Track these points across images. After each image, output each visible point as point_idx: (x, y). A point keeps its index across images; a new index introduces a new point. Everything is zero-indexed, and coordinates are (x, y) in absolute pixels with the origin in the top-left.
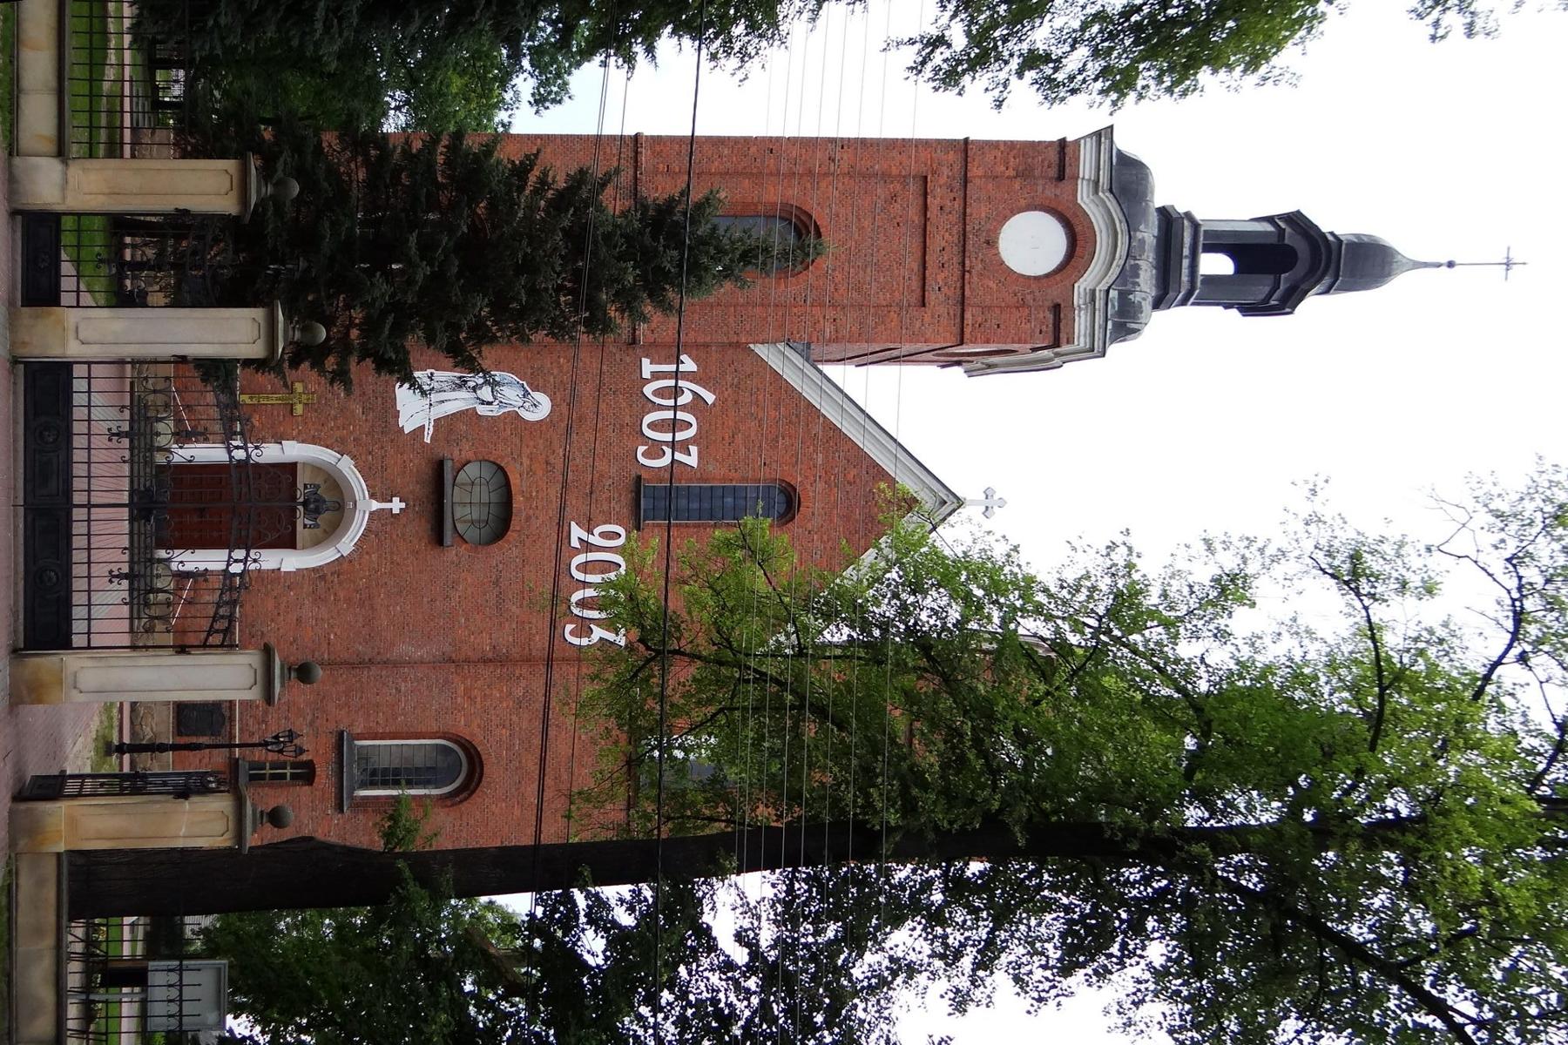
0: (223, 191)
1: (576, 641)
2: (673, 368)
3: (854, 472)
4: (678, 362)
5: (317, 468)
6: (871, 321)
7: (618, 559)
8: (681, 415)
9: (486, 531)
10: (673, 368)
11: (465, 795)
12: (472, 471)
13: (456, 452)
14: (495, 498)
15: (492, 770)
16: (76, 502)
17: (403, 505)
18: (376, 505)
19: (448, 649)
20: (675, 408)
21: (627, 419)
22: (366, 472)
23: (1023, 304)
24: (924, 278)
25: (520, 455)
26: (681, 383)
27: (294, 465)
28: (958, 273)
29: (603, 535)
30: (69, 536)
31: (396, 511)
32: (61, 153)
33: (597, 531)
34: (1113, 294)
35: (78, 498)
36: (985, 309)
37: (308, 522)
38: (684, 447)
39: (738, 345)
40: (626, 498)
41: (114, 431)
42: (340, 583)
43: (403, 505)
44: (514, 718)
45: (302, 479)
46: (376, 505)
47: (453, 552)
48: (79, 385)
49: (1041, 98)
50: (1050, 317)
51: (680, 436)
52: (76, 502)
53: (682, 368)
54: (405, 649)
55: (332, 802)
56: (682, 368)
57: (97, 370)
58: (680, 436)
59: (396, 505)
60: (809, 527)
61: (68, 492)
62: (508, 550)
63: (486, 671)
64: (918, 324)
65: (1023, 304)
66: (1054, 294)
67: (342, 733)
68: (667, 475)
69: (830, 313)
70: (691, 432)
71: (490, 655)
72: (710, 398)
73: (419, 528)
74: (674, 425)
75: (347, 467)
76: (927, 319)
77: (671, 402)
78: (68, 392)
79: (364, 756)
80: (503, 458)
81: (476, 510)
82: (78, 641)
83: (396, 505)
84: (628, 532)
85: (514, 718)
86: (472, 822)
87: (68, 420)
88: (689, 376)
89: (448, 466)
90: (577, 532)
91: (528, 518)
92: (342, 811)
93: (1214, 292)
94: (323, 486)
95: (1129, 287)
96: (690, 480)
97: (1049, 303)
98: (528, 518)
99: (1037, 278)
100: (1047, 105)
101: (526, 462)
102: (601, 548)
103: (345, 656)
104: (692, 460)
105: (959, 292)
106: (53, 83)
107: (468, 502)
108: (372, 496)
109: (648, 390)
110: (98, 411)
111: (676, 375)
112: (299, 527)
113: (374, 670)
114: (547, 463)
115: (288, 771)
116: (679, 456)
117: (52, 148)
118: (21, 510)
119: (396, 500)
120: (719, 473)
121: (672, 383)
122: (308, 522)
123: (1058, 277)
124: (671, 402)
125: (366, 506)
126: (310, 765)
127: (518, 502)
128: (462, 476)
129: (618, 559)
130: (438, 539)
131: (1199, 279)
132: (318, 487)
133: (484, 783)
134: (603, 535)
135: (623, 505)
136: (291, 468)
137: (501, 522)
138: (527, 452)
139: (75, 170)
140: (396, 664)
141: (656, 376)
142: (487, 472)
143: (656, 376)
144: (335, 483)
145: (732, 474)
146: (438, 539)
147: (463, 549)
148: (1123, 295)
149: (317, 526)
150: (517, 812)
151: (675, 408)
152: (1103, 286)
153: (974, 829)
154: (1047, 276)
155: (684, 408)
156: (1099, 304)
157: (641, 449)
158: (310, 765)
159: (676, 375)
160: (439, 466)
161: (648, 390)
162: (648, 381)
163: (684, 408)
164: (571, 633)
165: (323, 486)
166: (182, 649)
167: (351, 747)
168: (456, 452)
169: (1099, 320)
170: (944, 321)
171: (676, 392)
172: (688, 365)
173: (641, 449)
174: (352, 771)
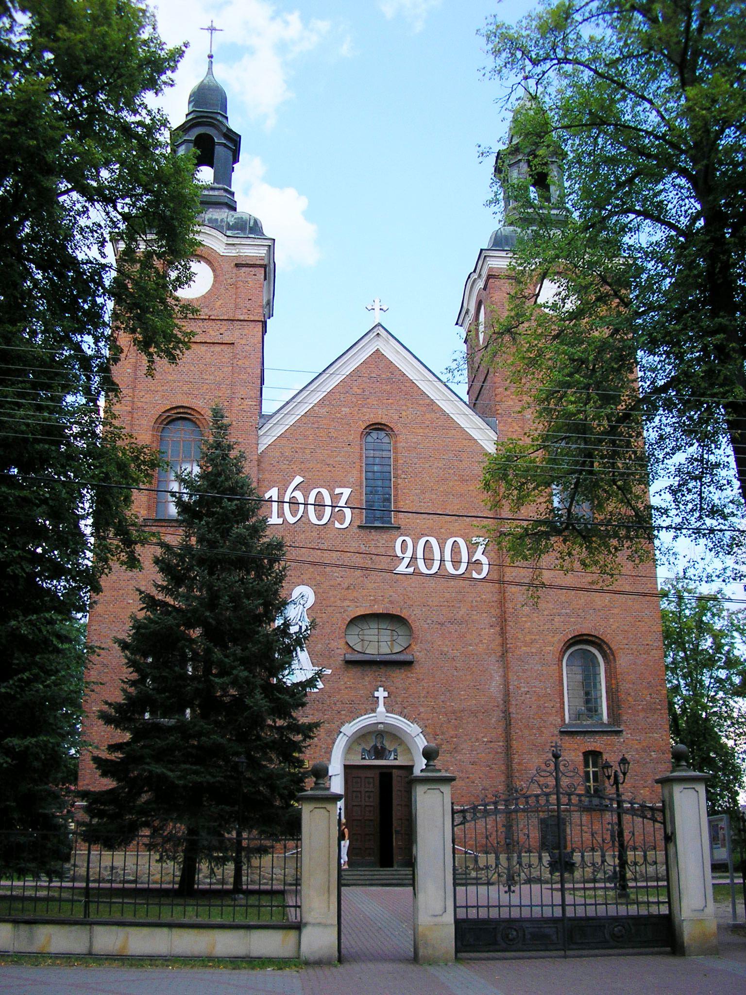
0: (327, 814)
1: (486, 568)
2: (275, 505)
3: (355, 389)
4: (270, 500)
5: (349, 749)
6: (244, 377)
7: (450, 542)
8: (311, 500)
9: (401, 630)
10: (275, 505)
11: (605, 646)
12: (353, 640)
13: (339, 651)
14: (374, 625)
15: (586, 627)
16: (560, 915)
17: (381, 689)
18: (381, 708)
19: (493, 659)
20: (306, 504)
21: (315, 534)
22: (354, 715)
23: (234, 285)
24: (214, 343)
25: (342, 607)
26: (287, 499)
27: (346, 767)
28: (210, 323)
29: (404, 551)
30: (587, 919)
31: (386, 694)
32: (298, 927)
33: (399, 554)
34: (229, 233)
35: (558, 912)
36: (236, 306)
37: (392, 757)
38: (335, 497)
39: (259, 462)
40: (374, 534)
41: (507, 889)
42: (443, 734)
43: (381, 689)
44: (546, 613)
45: (356, 760)
46: (381, 708)
47: (418, 653)
48: (472, 914)
49: (186, 286)
50: (244, 269)
51: (328, 501)
52: (560, 915)
53: (275, 498)
54: (495, 686)
55: (614, 738)
56: (275, 498)
57: (461, 902)
58: (328, 501)
59: (381, 694)
60: (397, 417)
61: (553, 920)
62: (411, 614)
63: (511, 631)
64: (248, 347)
65: (234, 285)
66: (228, 267)
67: (562, 732)
68: (356, 511)
69: (237, 401)
70: (325, 493)
71: (498, 629)
72: (298, 479)
73: (398, 677)
74: (319, 505)
75: (350, 729)
76: (243, 342)
77: (302, 507)
78: (478, 921)
79: (578, 716)
80: (344, 619)
81: (382, 638)
82: (664, 910)
83: (381, 694)
84: (402, 535)
85: (546, 613)
86: (625, 642)
87: (499, 922)
88: (282, 493)
89: (349, 657)
90: (402, 568)
91: (391, 602)
92: (621, 731)
93: (224, 177)
94: (364, 746)
95: (224, 224)
96: (361, 493)
97: (235, 270)
98: (391, 602)
99: (215, 276)
100: (191, 283)
101: (347, 603)
102: (413, 552)
103: (500, 731)
104: (347, 492)
105: (224, 323)
106: (242, 932)
107: (379, 643)
108: (374, 710)
109: (292, 520)
110: (491, 899)
111: (281, 502)
112: (396, 763)
113: (512, 710)
114: (348, 588)
115: (591, 769)
116: (342, 503)
117: (292, 934)
118: (569, 953)
119: (376, 694)
120: (354, 476)
121: (286, 506)
122: (392, 757)
123: (216, 264)
124: (302, 507)
125: (381, 715)
126: (586, 754)
127: (378, 609)
128: (358, 648)
129: (450, 542)
130: (407, 664)
131: (216, 185)
132: (364, 750)
133: (596, 633)
134: (404, 551)
135: (381, 538)
136: (347, 768)
137: (395, 620)
138: (339, 603)
139: (308, 917)
140: (507, 694)
141: (281, 514)
142: (355, 630)
143: (281, 514)
144: (362, 736)
145: (357, 466)
146: (407, 664)
147: (415, 648)
148: (230, 228)
149: (395, 751)
150: (616, 611)
151: (306, 504)
152: (225, 239)
153: (28, 220)
154: (214, 271)
155: (306, 497)
156: (236, 241)
157: (337, 525)
158: (586, 754)
159: (281, 502)
160: (349, 663)
161: (292, 520)
162: (285, 520)
163: (306, 497)
164: (479, 574)
165: (364, 746)
166: (670, 838)
167: (569, 725)
168: (339, 651)
169: (244, 241)
170: (246, 332)
171: (293, 503)
172: (273, 493)
173: (337, 525)
174: (587, 723)
